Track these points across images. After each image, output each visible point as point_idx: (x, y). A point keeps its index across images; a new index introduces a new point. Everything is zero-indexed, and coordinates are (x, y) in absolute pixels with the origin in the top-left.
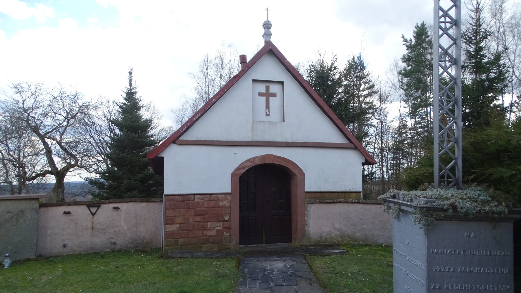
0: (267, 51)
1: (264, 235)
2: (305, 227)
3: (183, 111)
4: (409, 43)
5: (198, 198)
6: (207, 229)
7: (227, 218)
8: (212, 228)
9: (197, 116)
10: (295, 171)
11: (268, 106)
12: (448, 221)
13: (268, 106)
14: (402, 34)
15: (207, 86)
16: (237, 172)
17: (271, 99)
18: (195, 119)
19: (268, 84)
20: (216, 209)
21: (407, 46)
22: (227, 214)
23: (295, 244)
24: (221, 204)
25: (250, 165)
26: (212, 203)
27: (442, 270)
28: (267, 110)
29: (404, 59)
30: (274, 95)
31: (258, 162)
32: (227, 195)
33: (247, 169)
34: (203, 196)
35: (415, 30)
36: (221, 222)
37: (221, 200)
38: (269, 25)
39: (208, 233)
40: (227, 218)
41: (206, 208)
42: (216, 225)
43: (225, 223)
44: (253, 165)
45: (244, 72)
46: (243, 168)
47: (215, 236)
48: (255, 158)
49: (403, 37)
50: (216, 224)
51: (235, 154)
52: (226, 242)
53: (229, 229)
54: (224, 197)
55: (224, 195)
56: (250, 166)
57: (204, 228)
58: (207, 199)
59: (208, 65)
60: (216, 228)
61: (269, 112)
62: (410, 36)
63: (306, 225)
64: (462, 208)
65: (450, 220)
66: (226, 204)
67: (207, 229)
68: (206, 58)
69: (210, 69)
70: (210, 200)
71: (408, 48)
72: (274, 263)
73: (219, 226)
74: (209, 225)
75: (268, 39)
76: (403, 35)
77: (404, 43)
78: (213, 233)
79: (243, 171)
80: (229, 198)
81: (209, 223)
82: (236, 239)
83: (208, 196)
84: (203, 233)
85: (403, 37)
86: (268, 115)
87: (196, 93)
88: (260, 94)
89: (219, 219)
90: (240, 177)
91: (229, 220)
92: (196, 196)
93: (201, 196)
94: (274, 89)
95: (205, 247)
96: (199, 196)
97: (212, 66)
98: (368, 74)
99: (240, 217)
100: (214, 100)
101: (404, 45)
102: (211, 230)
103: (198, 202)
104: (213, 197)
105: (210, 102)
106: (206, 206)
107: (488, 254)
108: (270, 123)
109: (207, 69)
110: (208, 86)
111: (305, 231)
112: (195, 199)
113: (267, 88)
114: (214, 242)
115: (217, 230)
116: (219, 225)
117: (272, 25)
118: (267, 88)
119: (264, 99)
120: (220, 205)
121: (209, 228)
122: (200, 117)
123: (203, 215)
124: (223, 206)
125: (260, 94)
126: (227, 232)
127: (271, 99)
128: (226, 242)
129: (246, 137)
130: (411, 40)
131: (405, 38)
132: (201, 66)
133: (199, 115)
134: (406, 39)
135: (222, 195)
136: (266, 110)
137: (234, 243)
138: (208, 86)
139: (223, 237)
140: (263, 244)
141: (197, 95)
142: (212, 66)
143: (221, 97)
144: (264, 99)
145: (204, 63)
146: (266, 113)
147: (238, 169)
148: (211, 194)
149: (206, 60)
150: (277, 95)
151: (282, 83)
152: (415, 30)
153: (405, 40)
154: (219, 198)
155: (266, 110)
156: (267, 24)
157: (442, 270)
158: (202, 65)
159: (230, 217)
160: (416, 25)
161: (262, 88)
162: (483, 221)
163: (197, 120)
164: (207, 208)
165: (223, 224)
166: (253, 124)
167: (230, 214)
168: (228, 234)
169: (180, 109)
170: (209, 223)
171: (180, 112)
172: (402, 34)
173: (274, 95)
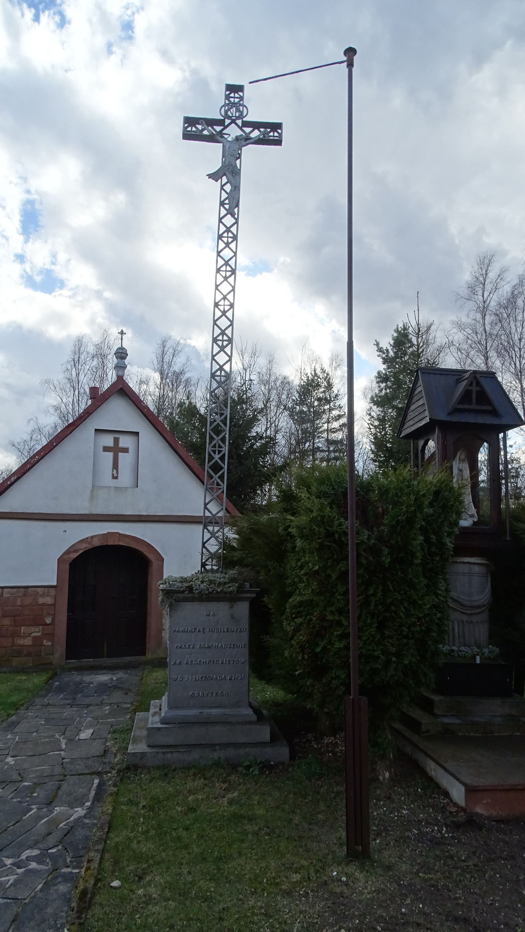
0: (117, 390)
1: (105, 645)
2: (161, 633)
3: (32, 445)
4: (386, 354)
5: (8, 593)
6: (20, 636)
7: (48, 621)
8: (27, 635)
9: (13, 479)
10: (151, 556)
11: (115, 466)
12: (190, 603)
13: (115, 466)
14: (376, 340)
15: (76, 403)
16: (66, 557)
17: (120, 454)
18: (9, 483)
19: (117, 436)
20: (34, 607)
21: (383, 358)
22: (49, 614)
23: (149, 656)
24: (41, 601)
25: (85, 546)
26: (28, 601)
27: (183, 647)
28: (115, 471)
29: (378, 378)
30: (125, 450)
31: (97, 543)
32: (50, 589)
33: (81, 552)
34: (16, 589)
35: (395, 335)
36: (41, 627)
37: (43, 596)
38: (123, 355)
39: (21, 642)
40: (48, 621)
41: (18, 606)
42: (33, 631)
43: (45, 627)
44: (90, 547)
45: (82, 420)
46: (76, 551)
47: (30, 646)
48: (92, 537)
49: (377, 344)
50: (33, 629)
51: (65, 531)
52: (46, 654)
53: (51, 636)
54: (46, 591)
55: (46, 589)
56: (85, 548)
57: (15, 635)
58: (21, 594)
59: (80, 367)
60: (33, 635)
61: (117, 473)
62: (387, 342)
63: (163, 630)
64: (197, 590)
65: (192, 601)
66: (49, 600)
67: (19, 636)
68: (76, 357)
69: (83, 375)
70: (25, 595)
71: (385, 361)
72: (99, 676)
73: (37, 631)
74: (22, 631)
75: (120, 374)
76: (378, 341)
77: (378, 353)
78: (28, 641)
79: (75, 555)
80: (53, 592)
81: (22, 628)
82: (60, 650)
83: (23, 589)
84: (13, 642)
85: (377, 344)
86: (115, 478)
87: (56, 414)
88: (106, 449)
89: (37, 621)
90: (70, 564)
91: (53, 623)
92: (5, 590)
93: (14, 590)
94: (125, 441)
95: (15, 662)
96: (9, 590)
97: (86, 371)
98: (337, 395)
99: (68, 620)
100: (37, 457)
101: (378, 356)
102: (24, 637)
103: (8, 598)
104: (30, 592)
105: (31, 460)
106: (19, 604)
107: (226, 631)
108: (117, 488)
109: (78, 375)
110: (79, 404)
111: (162, 637)
112: (4, 594)
113: (116, 440)
114: (29, 654)
115: (34, 638)
116: (37, 630)
117: (127, 355)
118: (116, 440)
119: (110, 455)
120: (40, 603)
121: (22, 635)
122: (15, 481)
123: (15, 616)
124: (43, 604)
125: (106, 449)
126: (48, 640)
127: (120, 454)
128: (46, 654)
129: (84, 508)
130: (387, 350)
131: (381, 346)
132: (67, 369)
133: (15, 478)
134: (382, 348)
135: (42, 589)
136: (113, 471)
137: (57, 655)
138: (79, 404)
139: (43, 647)
140: (103, 657)
141: (57, 418)
142: (86, 371)
143: (49, 452)
144: (110, 455)
145: (73, 364)
146: (113, 475)
147: (67, 552)
148: (27, 587)
149: (76, 359)
150: (130, 451)
151: (137, 434)
152: (395, 335)
153: (380, 350)
154: (38, 593)
155: (113, 471)
156: (120, 353)
157: (183, 647)
158: (69, 368)
159: (53, 620)
160: (395, 327)
161: (108, 441)
162: (222, 601)
163: (12, 484)
164: (20, 606)
165: (43, 629)
166: (92, 491)
167: (54, 615)
168: (50, 643)
169: (25, 441)
170: (22, 628)
171: (27, 447)
172: (376, 340)
173: (125, 450)
